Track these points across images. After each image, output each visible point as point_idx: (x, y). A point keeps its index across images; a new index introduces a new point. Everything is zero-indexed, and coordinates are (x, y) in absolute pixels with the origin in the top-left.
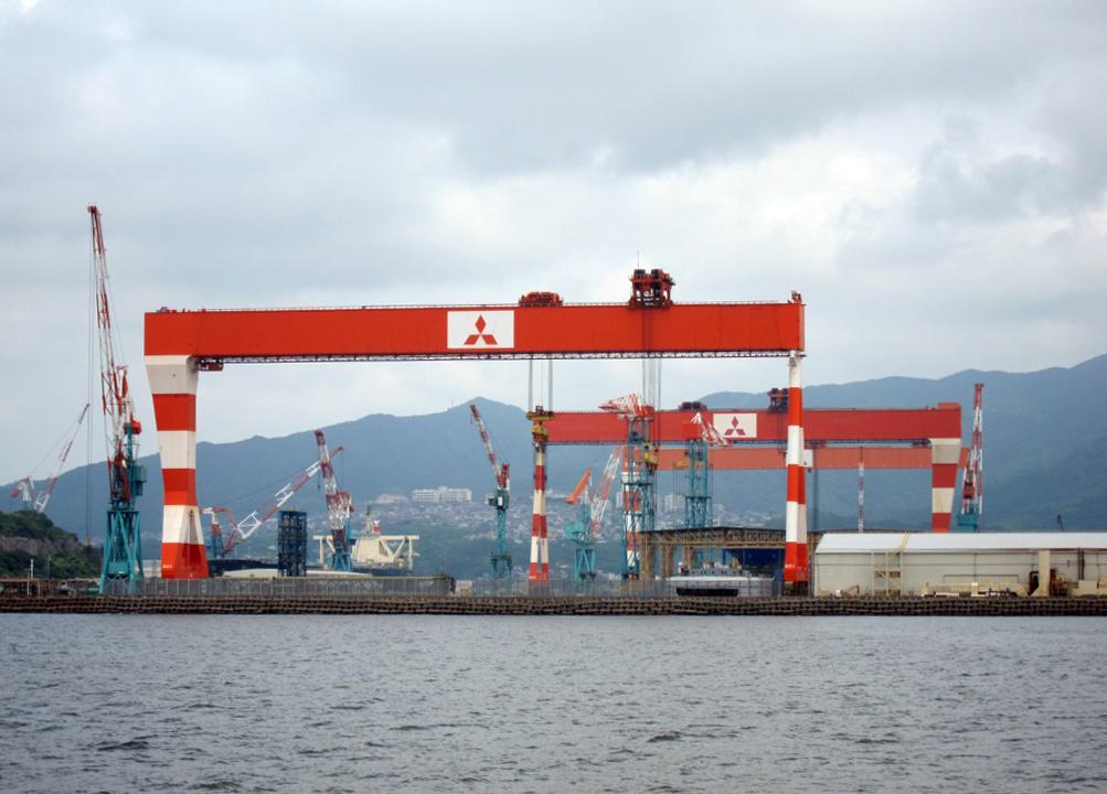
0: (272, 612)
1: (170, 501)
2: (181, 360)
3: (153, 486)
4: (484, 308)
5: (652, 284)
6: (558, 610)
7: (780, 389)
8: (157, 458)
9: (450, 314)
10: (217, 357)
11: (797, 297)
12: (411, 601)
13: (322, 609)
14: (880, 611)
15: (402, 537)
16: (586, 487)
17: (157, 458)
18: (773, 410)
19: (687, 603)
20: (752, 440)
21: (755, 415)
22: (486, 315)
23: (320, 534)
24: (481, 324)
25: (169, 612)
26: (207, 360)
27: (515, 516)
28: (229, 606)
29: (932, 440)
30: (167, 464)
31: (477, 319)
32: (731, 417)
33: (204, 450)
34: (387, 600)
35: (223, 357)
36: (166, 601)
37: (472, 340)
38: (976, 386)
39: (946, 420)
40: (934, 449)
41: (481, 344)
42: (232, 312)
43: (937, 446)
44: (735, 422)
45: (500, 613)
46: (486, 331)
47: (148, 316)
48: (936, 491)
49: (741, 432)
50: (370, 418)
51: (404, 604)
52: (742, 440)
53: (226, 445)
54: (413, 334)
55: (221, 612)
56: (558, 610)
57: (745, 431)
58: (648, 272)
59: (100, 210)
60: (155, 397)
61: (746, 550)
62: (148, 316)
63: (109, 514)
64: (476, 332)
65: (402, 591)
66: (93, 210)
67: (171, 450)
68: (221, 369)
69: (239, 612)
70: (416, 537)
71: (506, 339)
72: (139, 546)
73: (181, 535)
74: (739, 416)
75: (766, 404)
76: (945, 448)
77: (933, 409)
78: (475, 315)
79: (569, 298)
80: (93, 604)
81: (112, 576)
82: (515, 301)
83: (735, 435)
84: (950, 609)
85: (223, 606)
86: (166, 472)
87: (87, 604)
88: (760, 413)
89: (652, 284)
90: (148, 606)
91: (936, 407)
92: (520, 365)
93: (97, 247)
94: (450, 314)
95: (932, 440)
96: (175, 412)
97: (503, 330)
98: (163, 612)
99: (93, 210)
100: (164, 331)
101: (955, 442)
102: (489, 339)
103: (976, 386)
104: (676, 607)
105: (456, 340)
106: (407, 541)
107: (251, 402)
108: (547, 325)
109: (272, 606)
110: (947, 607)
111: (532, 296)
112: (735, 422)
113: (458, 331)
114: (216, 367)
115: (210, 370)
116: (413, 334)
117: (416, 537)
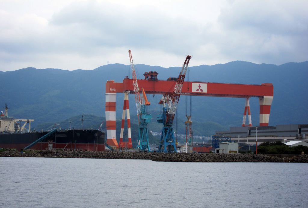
15: (26, 120)
21: (206, 84)
23: (26, 118)
29: (264, 96)
32: (198, 84)
37: (198, 90)
39: (268, 89)
40: (265, 100)
41: (200, 91)
43: (266, 99)
44: (200, 86)
46: (201, 88)
49: (202, 90)
50: (23, 69)
64: (198, 88)
65: (42, 143)
70: (33, 120)
71: (205, 91)
73: (262, 117)
74: (201, 84)
76: (268, 100)
94: (193, 84)
95: (264, 96)
101: (272, 97)
106: (28, 122)
112: (200, 86)
117: (33, 120)
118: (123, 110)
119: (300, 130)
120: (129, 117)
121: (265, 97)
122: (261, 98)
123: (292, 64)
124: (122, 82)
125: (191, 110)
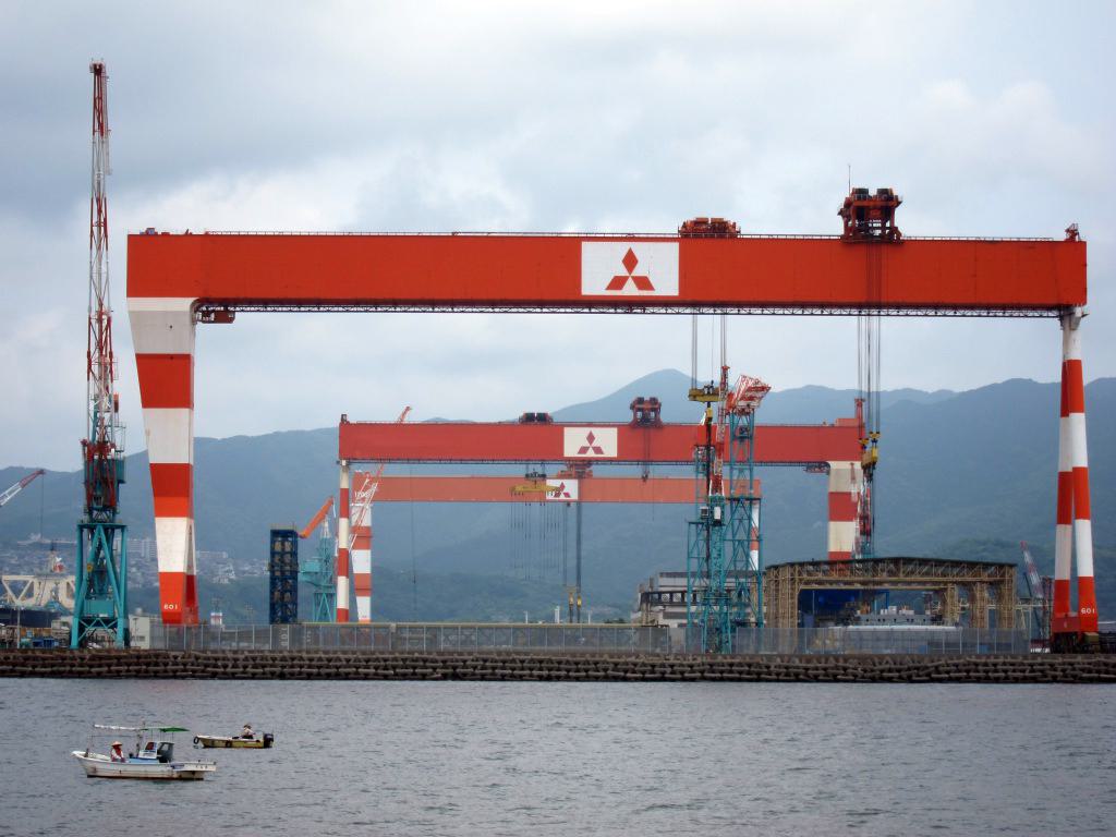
0: (456, 677)
1: (164, 511)
2: (184, 304)
3: (134, 493)
4: (631, 238)
5: (869, 211)
6: (904, 674)
7: (647, 398)
8: (145, 454)
9: (586, 247)
10: (226, 302)
11: (1073, 232)
12: (672, 661)
13: (535, 673)
14: (774, 677)
16: (327, 518)
17: (145, 454)
18: (635, 425)
19: (1098, 664)
20: (610, 461)
21: (615, 430)
22: (639, 249)
24: (630, 261)
25: (292, 676)
26: (217, 307)
27: (13, 562)
28: (386, 668)
30: (153, 460)
31: (626, 251)
32: (587, 430)
33: (200, 444)
34: (633, 659)
35: (238, 302)
36: (283, 659)
37: (618, 283)
38: (857, 400)
41: (630, 290)
42: (256, 236)
43: (838, 471)
44: (591, 438)
45: (816, 679)
46: (638, 271)
47: (131, 237)
48: (834, 526)
49: (598, 450)
51: (663, 665)
52: (597, 460)
53: (266, 436)
54: (526, 273)
55: (376, 677)
56: (904, 674)
57: (603, 449)
58: (873, 192)
59: (108, 71)
60: (140, 358)
61: (817, 591)
62: (131, 237)
63: (81, 527)
64: (623, 272)
66: (98, 71)
67: (146, 435)
68: (230, 320)
69: (404, 677)
71: (667, 283)
72: (579, 558)
74: (596, 431)
75: (628, 417)
76: (844, 474)
77: (833, 426)
78: (623, 248)
79: (749, 227)
80: (166, 664)
81: (89, 621)
82: (673, 229)
83: (591, 454)
84: (229, 670)
85: (376, 668)
86: (153, 466)
87: (157, 664)
88: (622, 428)
89: (869, 211)
90: (255, 667)
91: (837, 424)
92: (678, 324)
93: (97, 127)
94: (583, 243)
96: (167, 381)
97: (663, 271)
98: (282, 676)
99: (98, 71)
100: (159, 263)
102: (643, 283)
103: (857, 400)
104: (1083, 670)
105: (594, 282)
107: (284, 377)
108: (725, 267)
109: (455, 668)
110: (475, 668)
111: (699, 222)
112: (591, 438)
113: (596, 272)
114: (224, 318)
115: (217, 321)
116: (526, 273)
118: (192, 463)
119: (1114, 666)
120: (1086, 569)
121: (834, 465)
122: (822, 466)
123: (821, 390)
124: (160, 233)
125: (579, 558)
